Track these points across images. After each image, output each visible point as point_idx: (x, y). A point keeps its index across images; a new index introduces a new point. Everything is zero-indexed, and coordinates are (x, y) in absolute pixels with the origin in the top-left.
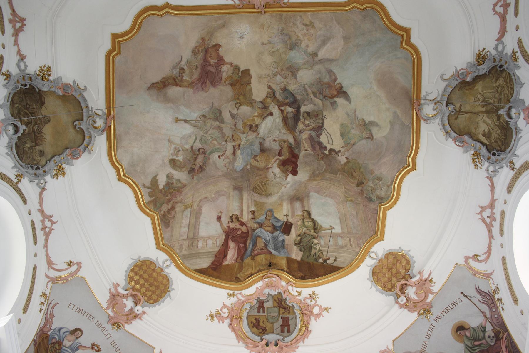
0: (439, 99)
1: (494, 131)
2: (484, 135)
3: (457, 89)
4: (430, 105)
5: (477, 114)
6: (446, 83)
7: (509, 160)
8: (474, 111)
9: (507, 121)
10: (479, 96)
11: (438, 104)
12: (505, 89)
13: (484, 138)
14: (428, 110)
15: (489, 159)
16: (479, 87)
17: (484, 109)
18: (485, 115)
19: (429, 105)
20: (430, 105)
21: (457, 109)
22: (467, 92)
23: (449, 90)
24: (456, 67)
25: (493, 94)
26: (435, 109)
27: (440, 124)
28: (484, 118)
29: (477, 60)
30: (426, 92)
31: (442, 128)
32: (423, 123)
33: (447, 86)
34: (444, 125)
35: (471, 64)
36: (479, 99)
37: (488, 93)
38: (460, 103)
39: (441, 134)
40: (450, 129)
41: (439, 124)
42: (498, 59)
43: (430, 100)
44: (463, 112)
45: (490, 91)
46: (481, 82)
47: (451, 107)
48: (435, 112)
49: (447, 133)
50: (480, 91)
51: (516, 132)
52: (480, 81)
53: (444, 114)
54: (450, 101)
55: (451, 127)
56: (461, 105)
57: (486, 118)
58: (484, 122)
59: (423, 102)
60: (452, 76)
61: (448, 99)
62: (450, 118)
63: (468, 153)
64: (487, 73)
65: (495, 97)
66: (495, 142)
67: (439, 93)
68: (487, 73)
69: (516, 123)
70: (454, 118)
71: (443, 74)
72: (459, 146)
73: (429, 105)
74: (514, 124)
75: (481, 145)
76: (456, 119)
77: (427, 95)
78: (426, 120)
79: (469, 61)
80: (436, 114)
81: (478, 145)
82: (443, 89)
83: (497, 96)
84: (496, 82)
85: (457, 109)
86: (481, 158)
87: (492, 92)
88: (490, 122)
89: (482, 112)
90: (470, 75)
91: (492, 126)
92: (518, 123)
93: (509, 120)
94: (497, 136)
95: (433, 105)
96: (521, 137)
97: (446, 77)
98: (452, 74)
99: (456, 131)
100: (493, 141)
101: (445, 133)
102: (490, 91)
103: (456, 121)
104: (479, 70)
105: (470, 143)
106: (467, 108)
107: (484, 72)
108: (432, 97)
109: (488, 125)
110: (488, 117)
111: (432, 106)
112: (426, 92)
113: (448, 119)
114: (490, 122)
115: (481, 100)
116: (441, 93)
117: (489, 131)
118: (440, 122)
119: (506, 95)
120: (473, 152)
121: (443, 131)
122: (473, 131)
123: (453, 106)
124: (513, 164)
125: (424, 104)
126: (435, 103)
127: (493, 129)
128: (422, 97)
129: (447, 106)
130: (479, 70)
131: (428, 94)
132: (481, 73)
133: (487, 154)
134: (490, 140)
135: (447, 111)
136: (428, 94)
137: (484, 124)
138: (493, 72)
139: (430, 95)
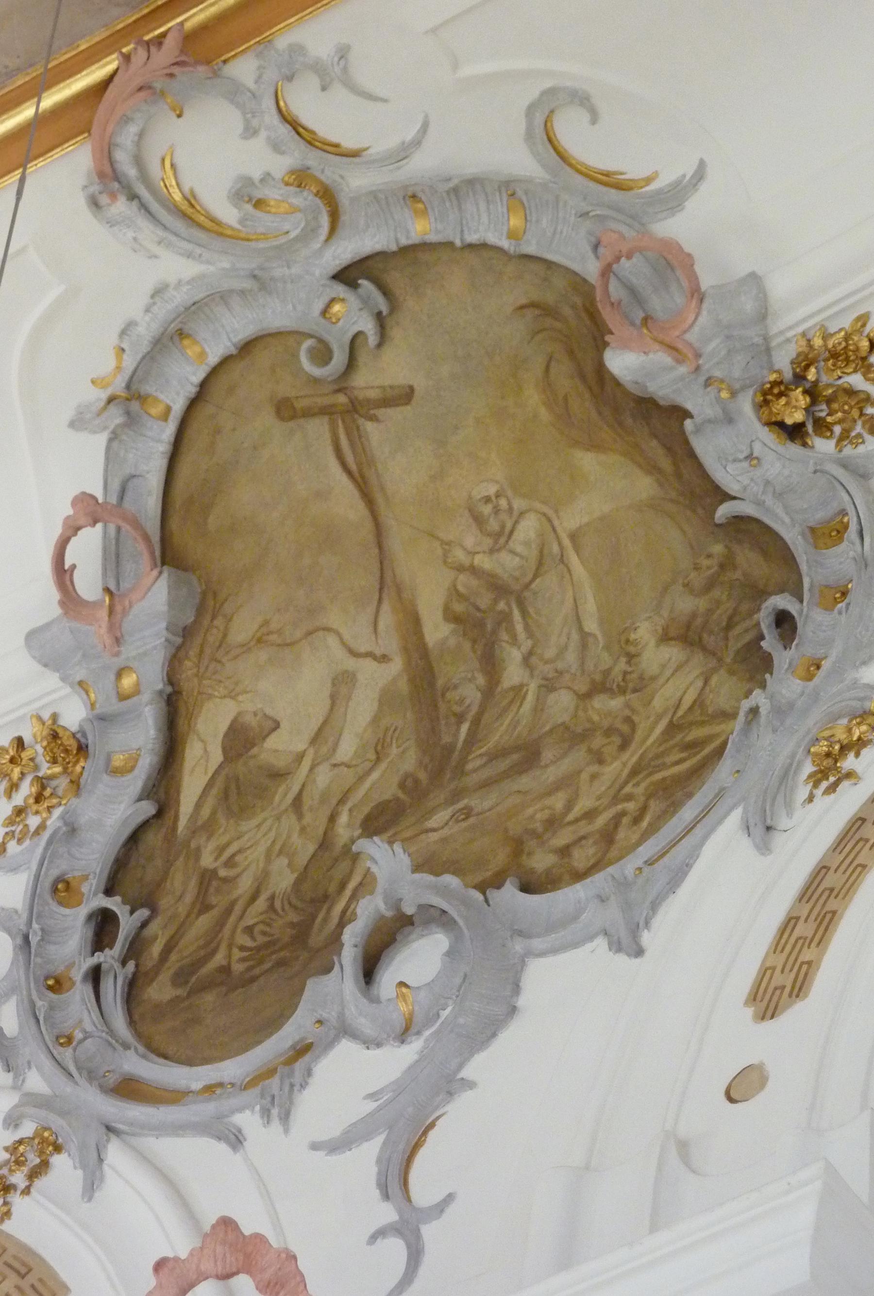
0: (355, 181)
1: (290, 821)
2: (240, 740)
3: (515, 294)
4: (259, 144)
5: (387, 583)
6: (521, 161)
7: (57, 1122)
8: (395, 543)
9: (335, 941)
10: (528, 529)
11: (305, 199)
12: (614, 769)
13: (217, 757)
14: (210, 148)
15: (63, 889)
16: (609, 486)
17: (436, 631)
18: (397, 665)
19: (249, 132)
20: (259, 144)
21: (368, 380)
22: (533, 397)
23: (487, 225)
24: (700, 174)
25: (571, 658)
26: (248, 195)
27: (164, 310)
28: (367, 669)
29: (804, 362)
30: (343, 53)
31: (147, 329)
32: (65, 172)
33: (510, 190)
34: (175, 335)
35: (763, 315)
36: (500, 539)
37: (573, 605)
38: (420, 383)
39: (92, 362)
40: (178, 406)
41: (159, 292)
42: (839, 560)
43: (295, 126)
44: (356, 437)
45: (590, 606)
46: (644, 486)
47: (353, 315)
48: (228, 214)
49: (130, 400)
50: (571, 519)
51: (270, 1072)
52: (652, 469)
53: (262, 283)
54: (396, 279)
55: (193, 404)
56: (404, 396)
57: (375, 679)
58: (342, 685)
59: (243, 68)
60: (608, 180)
61: (410, 253)
62: (263, 358)
63: (52, 680)
64: (723, 511)
65: (549, 686)
66: (207, 877)
67: (404, 152)
68: (723, 511)
69: (346, 1031)
70: (286, 388)
71: (581, 99)
72: (62, 573)
73: (249, 132)
74: (330, 1014)
75: (147, 763)
76: (286, 410)
77: (318, 69)
78: (111, 182)
79: (780, 286)
80: (215, 228)
81: (142, 736)
82: (471, 170)
83: (561, 705)
84: (665, 638)
85: (368, 380)
86: (54, 820)
87: (584, 636)
88: (347, 749)
89: (412, 623)
90: (662, 358)
91: (323, 777)
92: (346, 1047)
93: (349, 955)
94: (245, 884)
95: (280, 165)
96: (236, 1140)
97: (572, 131)
98: (633, 171)
99: (184, 470)
100: (207, 860)
101: (118, 386)
102: (590, 606)
103: (267, 419)
104: (729, 420)
105: (129, 651)
106: (402, 460)
107: (727, 477)
108: (328, 114)
109: (323, 735)
110: (387, 699)
111: (264, 158)
112: (343, 53)
113: (247, 348)
114: (347, 749)
115: (505, 564)
116: (423, 164)
117: (278, 775)
118: (178, 298)
119: (558, 802)
120: (73, 715)
121: (129, 363)
122: (243, 628)
123: (368, 326)
124: (43, 1167)
125: (235, 93)
126: (300, 178)
127: (297, 802)
128: (282, 42)
129: (347, 276)
130: (729, 420)
131: (336, 73)
132: (714, 449)
133: (93, 857)
134: (208, 828)
135: (302, 297)
136: (336, 73)
137: (315, 694)
138: (749, 561)
139: (339, 92)
